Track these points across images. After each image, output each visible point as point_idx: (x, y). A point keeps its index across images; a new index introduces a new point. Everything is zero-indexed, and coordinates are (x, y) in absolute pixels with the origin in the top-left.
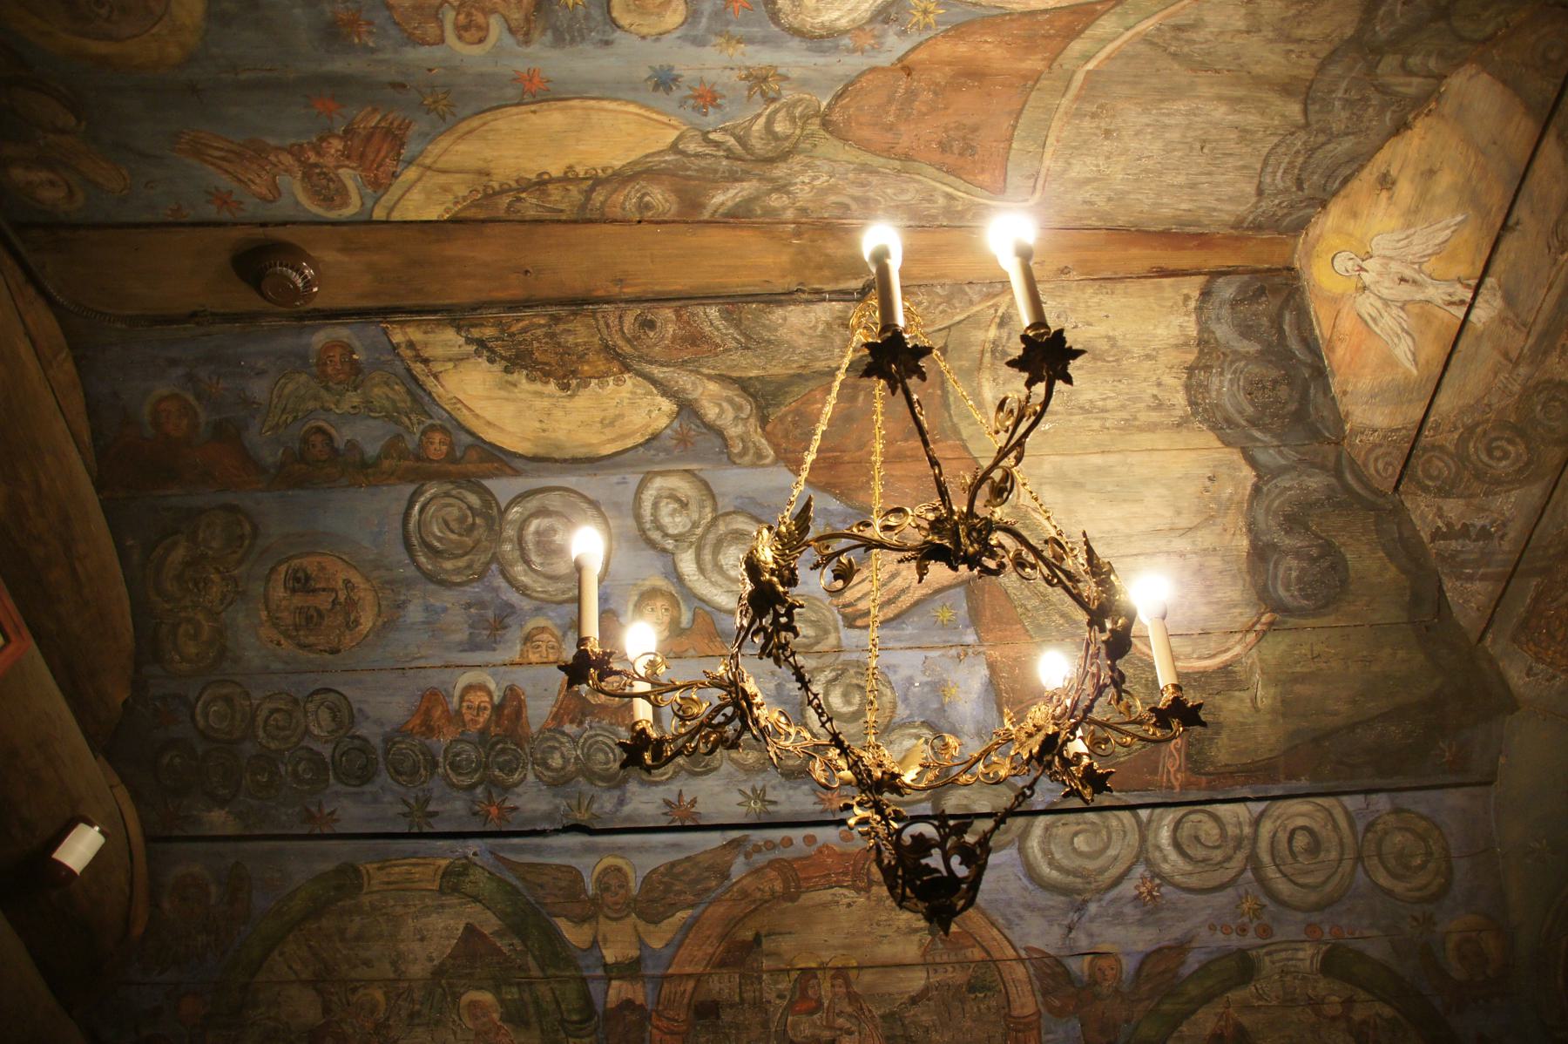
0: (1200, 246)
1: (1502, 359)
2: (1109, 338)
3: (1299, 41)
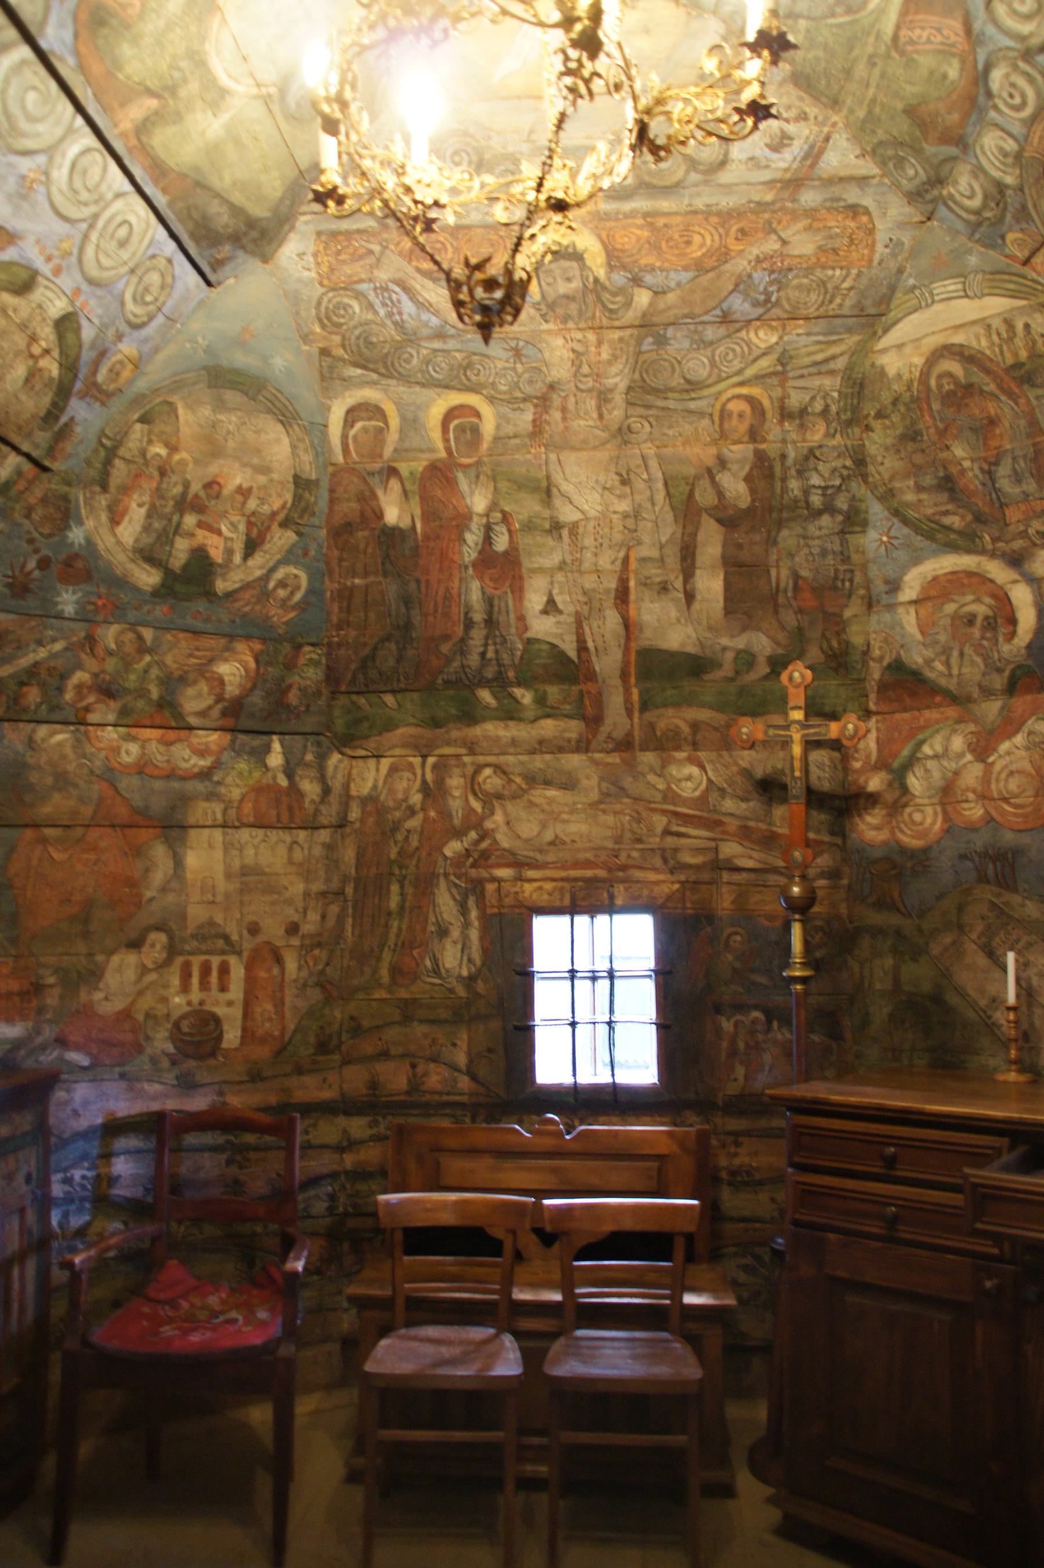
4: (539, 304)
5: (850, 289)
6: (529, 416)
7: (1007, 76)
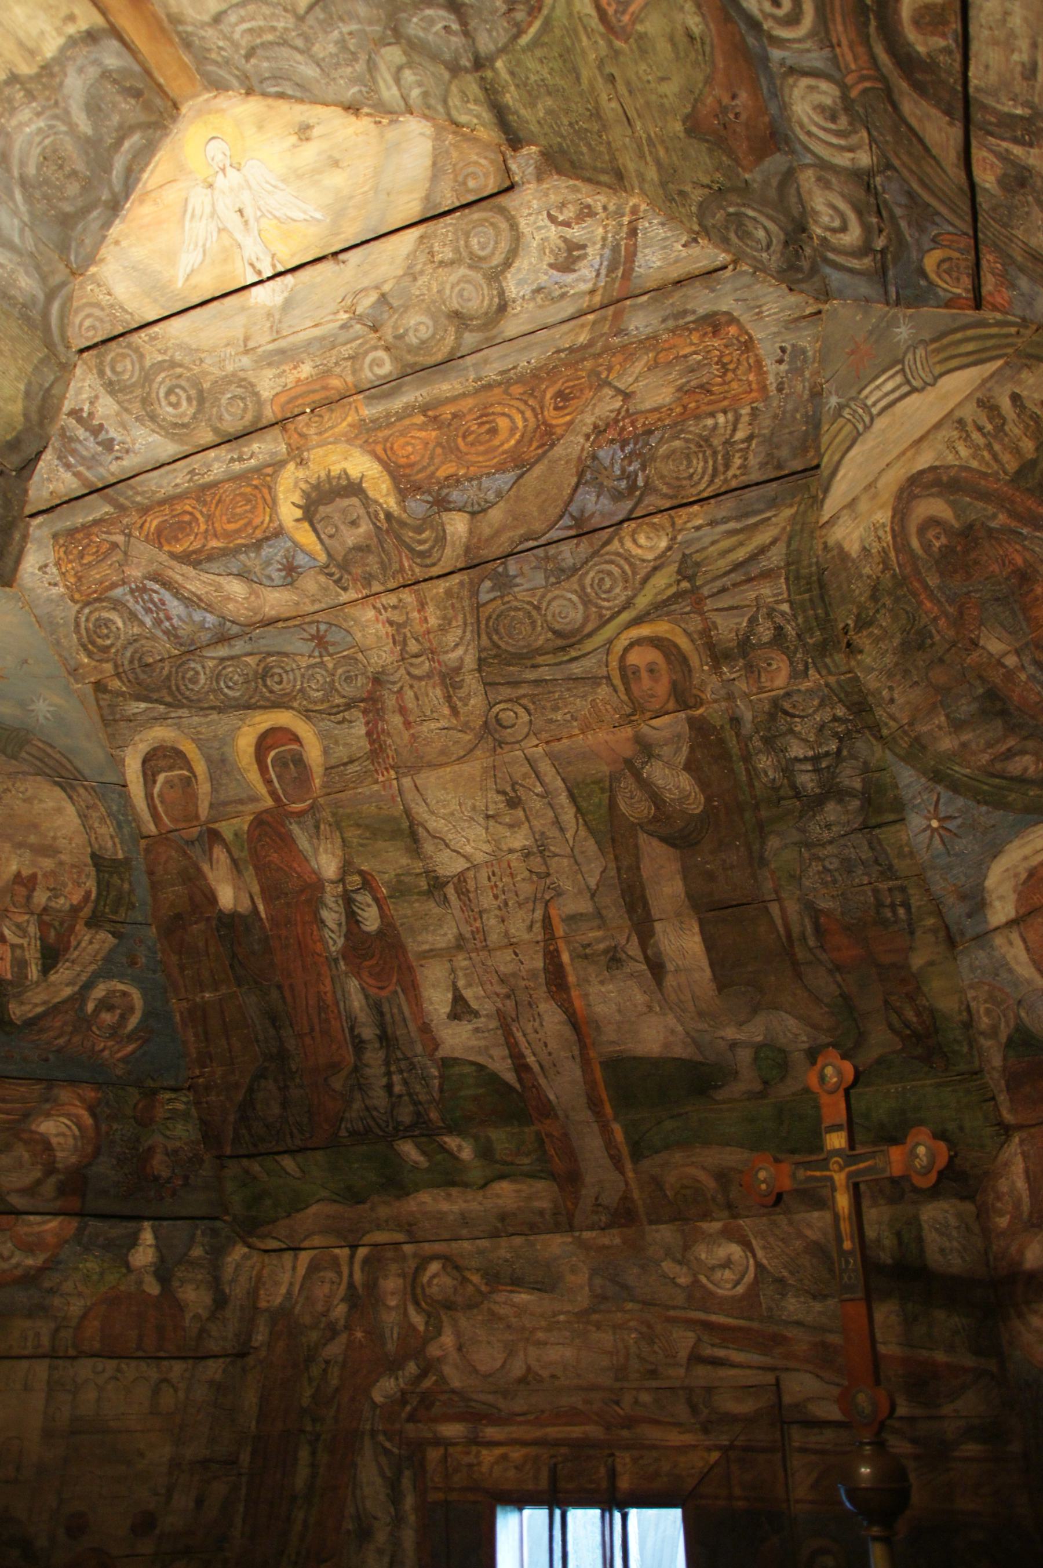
1: (242, 339)
4: (327, 566)
5: (750, 438)
6: (360, 729)
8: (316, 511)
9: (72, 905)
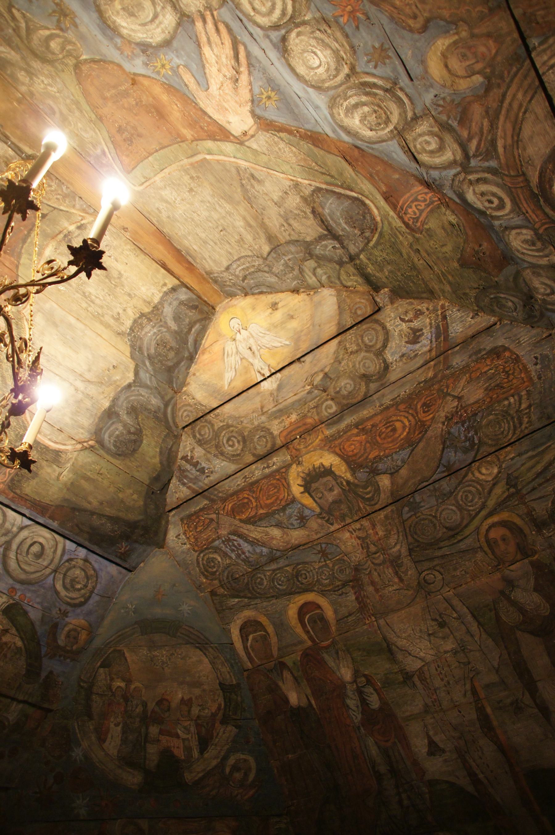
0: (187, 268)
1: (260, 407)
2: (120, 273)
3: (290, 225)
4: (321, 514)
5: (529, 406)
7: (475, 193)
8: (311, 487)
9: (212, 713)
